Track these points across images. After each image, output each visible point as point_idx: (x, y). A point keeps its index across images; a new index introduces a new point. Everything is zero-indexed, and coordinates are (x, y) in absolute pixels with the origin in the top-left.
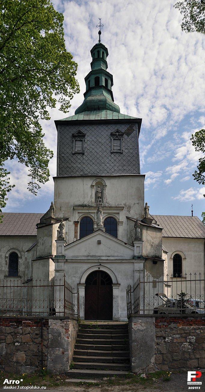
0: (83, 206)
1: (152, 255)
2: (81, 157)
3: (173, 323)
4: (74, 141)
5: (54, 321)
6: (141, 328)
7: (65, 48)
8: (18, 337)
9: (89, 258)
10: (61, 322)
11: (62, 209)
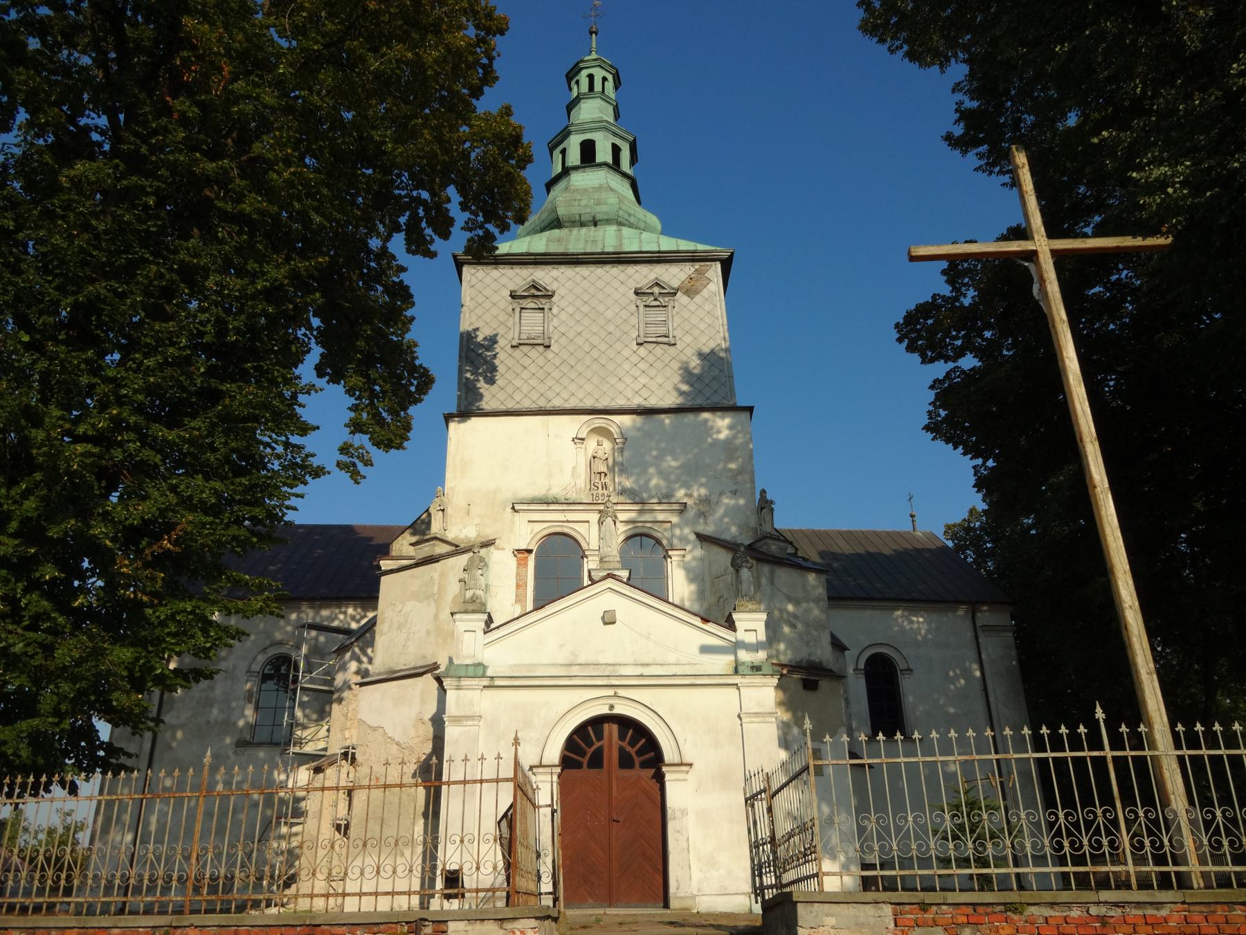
0: (547, 502)
2: (538, 354)
4: (518, 310)
5: (470, 928)
7: (486, 89)
9: (575, 671)
11: (473, 509)
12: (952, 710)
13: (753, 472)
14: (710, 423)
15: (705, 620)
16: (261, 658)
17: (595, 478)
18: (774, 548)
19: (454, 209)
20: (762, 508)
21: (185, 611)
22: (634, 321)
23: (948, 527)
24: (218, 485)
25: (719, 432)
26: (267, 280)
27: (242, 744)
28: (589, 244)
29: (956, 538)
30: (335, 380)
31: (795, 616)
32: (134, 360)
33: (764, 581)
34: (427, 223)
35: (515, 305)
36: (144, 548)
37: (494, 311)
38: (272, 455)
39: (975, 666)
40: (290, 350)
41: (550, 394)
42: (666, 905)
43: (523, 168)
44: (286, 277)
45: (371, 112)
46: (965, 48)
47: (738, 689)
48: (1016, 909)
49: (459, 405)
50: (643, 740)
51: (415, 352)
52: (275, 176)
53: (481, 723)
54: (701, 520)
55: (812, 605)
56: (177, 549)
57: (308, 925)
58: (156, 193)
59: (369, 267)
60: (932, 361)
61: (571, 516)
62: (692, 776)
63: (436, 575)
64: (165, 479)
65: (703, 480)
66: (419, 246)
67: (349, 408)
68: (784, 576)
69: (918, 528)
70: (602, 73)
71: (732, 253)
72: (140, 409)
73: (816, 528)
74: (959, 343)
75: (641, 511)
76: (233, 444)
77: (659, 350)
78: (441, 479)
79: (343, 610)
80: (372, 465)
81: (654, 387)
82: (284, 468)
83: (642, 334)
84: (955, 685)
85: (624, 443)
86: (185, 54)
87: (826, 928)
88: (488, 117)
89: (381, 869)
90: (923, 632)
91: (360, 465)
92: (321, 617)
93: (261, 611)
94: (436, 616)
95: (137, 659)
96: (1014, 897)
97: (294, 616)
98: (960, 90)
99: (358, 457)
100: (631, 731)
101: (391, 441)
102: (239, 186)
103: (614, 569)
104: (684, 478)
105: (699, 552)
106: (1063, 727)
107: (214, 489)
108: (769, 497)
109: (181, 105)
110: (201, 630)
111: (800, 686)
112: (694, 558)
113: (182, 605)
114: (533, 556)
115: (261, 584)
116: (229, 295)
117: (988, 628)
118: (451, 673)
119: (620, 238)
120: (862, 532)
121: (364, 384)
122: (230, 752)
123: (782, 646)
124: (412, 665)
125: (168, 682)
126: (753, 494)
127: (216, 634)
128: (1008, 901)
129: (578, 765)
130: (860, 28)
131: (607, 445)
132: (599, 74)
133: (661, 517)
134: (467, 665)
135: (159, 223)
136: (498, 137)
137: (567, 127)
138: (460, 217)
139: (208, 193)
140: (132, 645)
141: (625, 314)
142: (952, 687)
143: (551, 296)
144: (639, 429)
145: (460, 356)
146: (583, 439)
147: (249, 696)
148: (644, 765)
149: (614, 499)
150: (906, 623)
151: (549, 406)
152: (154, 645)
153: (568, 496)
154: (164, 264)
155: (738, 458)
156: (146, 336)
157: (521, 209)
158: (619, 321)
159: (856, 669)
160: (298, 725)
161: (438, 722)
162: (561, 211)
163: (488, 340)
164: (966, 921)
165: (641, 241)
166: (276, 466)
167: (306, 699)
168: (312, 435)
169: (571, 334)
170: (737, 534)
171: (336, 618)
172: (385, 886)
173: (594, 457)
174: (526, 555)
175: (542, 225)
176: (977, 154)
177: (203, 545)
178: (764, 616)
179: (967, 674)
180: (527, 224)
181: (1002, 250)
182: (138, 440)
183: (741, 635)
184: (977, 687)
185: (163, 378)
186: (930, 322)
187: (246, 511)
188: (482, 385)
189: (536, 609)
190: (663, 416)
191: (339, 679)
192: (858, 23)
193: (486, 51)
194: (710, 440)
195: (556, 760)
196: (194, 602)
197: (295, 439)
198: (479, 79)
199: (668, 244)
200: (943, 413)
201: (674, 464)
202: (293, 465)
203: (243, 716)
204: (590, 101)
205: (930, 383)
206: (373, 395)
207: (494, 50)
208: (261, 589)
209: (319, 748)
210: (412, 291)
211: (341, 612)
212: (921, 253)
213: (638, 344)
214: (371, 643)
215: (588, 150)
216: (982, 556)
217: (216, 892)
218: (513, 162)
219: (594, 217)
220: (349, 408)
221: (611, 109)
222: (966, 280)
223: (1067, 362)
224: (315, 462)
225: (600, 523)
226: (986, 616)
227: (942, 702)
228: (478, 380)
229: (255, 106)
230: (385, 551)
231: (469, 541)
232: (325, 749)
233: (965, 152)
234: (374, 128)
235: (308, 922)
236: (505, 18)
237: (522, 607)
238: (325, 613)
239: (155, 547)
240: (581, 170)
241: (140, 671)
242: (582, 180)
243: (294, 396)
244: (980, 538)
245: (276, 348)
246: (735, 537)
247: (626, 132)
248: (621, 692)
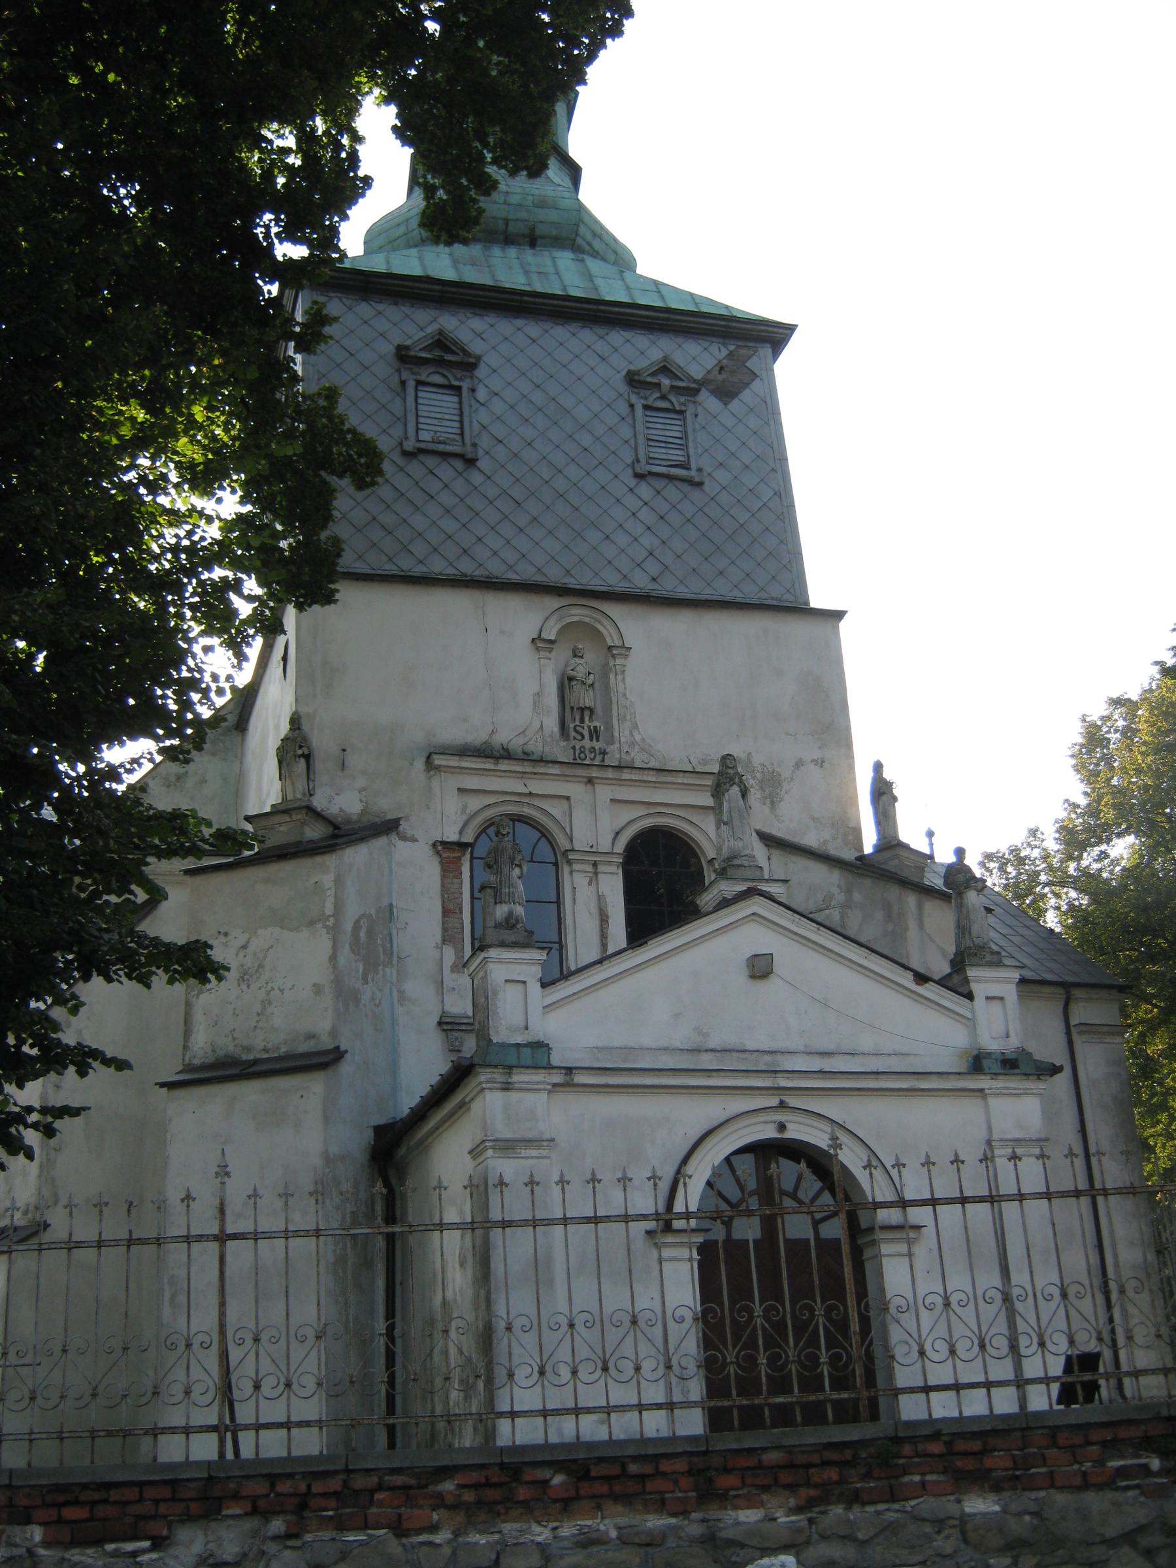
4: (411, 385)
11: (352, 760)
22: (625, 431)
35: (405, 375)
61: (537, 787)
63: (328, 880)
77: (672, 492)
94: (333, 958)
134: (518, 1045)
146: (552, 642)
153: (530, 748)
173: (571, 679)
237: (456, 952)
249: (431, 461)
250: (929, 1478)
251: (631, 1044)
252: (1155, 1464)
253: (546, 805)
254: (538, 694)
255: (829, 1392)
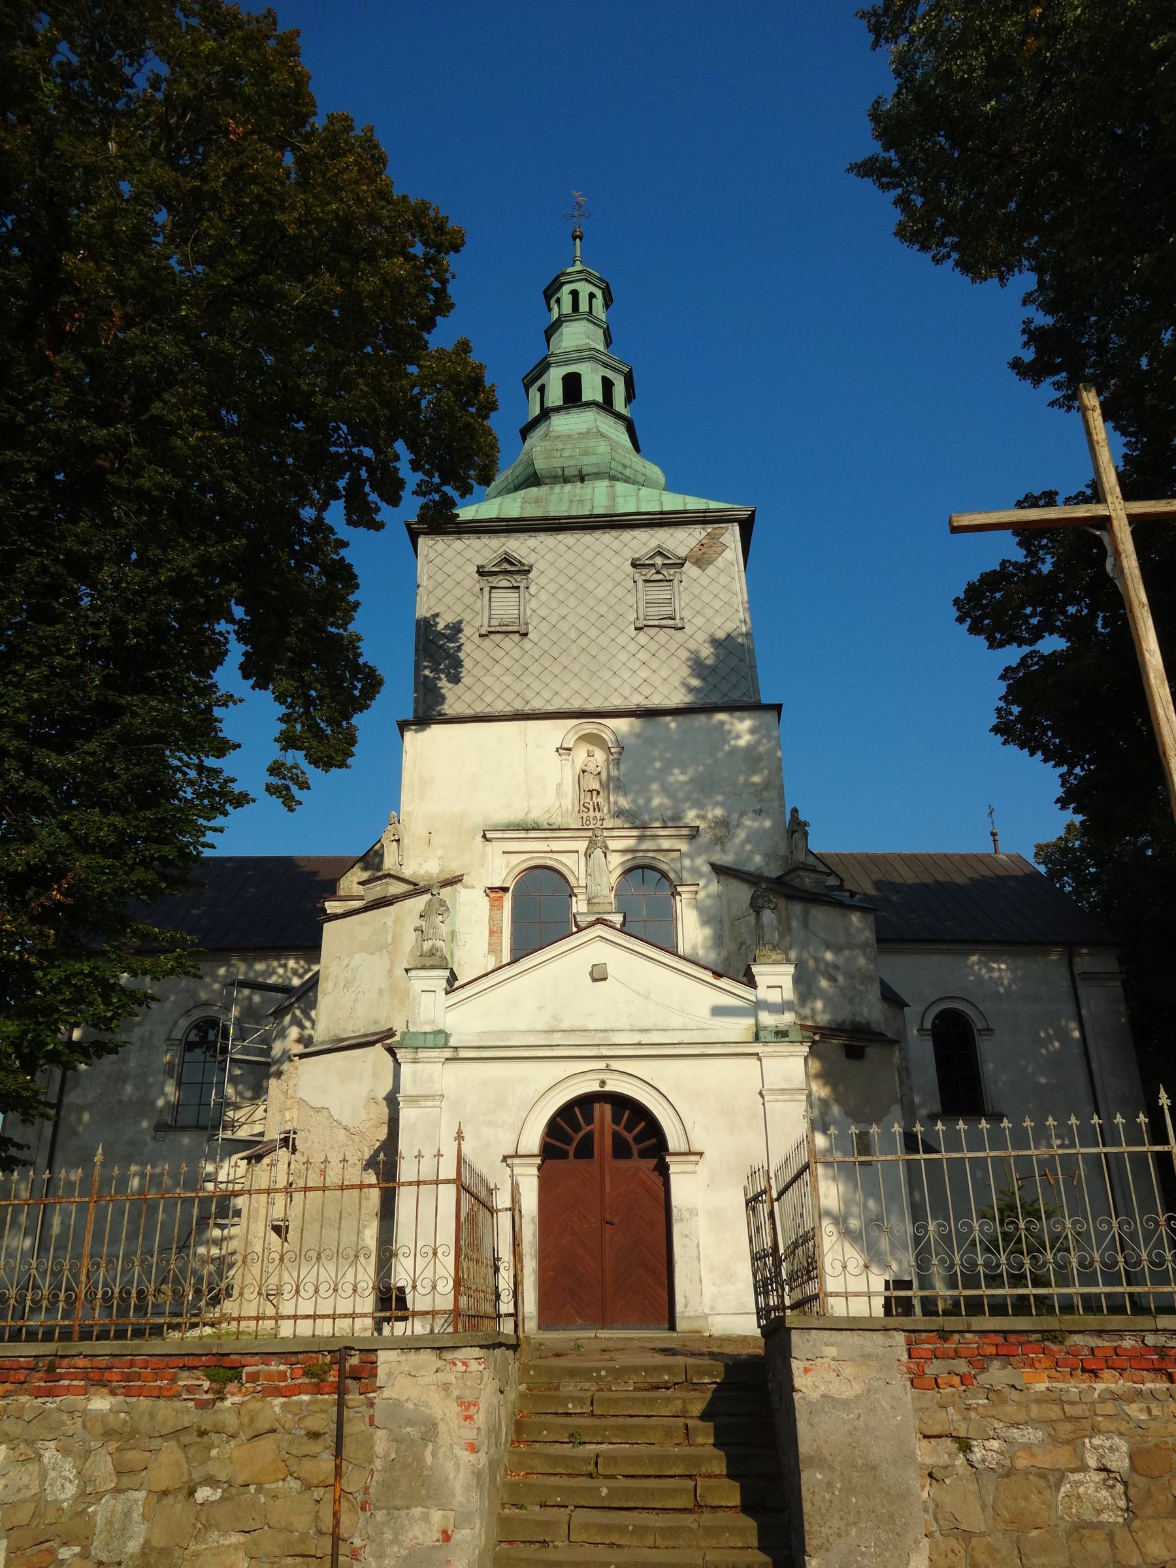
0: (526, 828)
1: (840, 1020)
2: (513, 644)
3: (996, 1364)
4: (487, 589)
5: (403, 1358)
6: (844, 1391)
7: (439, 319)
8: (214, 1452)
9: (557, 1039)
10: (440, 1363)
11: (435, 839)
12: (1043, 1080)
13: (782, 787)
14: (727, 727)
15: (718, 975)
16: (184, 1023)
17: (586, 797)
18: (808, 881)
19: (404, 468)
20: (793, 832)
21: (82, 972)
22: (630, 599)
23: (1040, 848)
24: (117, 820)
25: (738, 737)
26: (172, 570)
27: (162, 1128)
28: (575, 504)
29: (1050, 861)
30: (261, 685)
31: (835, 967)
32: (15, 673)
33: (795, 924)
34: (371, 486)
35: (483, 584)
36: (30, 900)
37: (458, 592)
38: (183, 781)
39: (1073, 1025)
40: (203, 652)
41: (529, 694)
42: (672, 1327)
43: (486, 417)
44: (194, 566)
45: (295, 357)
46: (1032, 254)
47: (760, 1059)
48: (1056, 1338)
49: (416, 710)
50: (643, 1124)
51: (359, 648)
52: (179, 442)
53: (443, 1104)
54: (718, 848)
55: (857, 952)
56: (70, 901)
57: (214, 1355)
58: (37, 468)
59: (301, 543)
60: (1001, 645)
62: (703, 1167)
63: (390, 921)
64: (55, 815)
65: (720, 798)
66: (362, 516)
67: (279, 719)
68: (820, 915)
69: (1001, 849)
70: (591, 289)
71: (753, 512)
72: (20, 731)
73: (871, 851)
74: (1034, 621)
75: (641, 838)
76: (136, 770)
77: (662, 636)
78: (394, 801)
79: (283, 962)
80: (308, 788)
81: (656, 680)
82: (200, 796)
83: (641, 617)
84: (1047, 1049)
85: (620, 753)
86: (66, 299)
87: (825, 1360)
88: (441, 354)
89: (301, 1288)
90: (1006, 982)
91: (294, 789)
92: (255, 971)
93: (171, 972)
94: (390, 971)
95: (25, 1032)
96: (1050, 1323)
97: (222, 971)
98: (1033, 302)
99: (292, 779)
100: (627, 1112)
101: (331, 758)
102: (136, 455)
103: (605, 913)
104: (695, 796)
105: (715, 887)
106: (1118, 1116)
107: (114, 825)
108: (802, 817)
109: (64, 360)
110: (101, 995)
111: (841, 1054)
112: (709, 896)
113: (78, 966)
114: (509, 895)
115: (173, 938)
116: (127, 588)
117: (1088, 976)
118: (407, 1043)
119: (613, 497)
120: (929, 855)
121: (296, 689)
122: (149, 1138)
123: (819, 1005)
124: (361, 1032)
125: (64, 1059)
126: (783, 813)
127: (120, 1000)
128: (1045, 1328)
129: (563, 1155)
130: (896, 234)
131: (600, 756)
132: (584, 289)
133: (666, 844)
135: (41, 505)
136: (453, 381)
137: (546, 358)
138: (411, 478)
139: (101, 462)
140: (19, 1016)
141: (619, 591)
142: (1043, 1051)
143: (528, 571)
144: (638, 736)
145: (416, 650)
146: (569, 749)
147: (169, 1070)
148: (643, 1154)
149: (609, 823)
150: (984, 971)
151: (527, 709)
152: (46, 1016)
153: (552, 821)
154: (48, 554)
155: (763, 768)
156: (28, 642)
157: (485, 466)
158: (613, 601)
159: (921, 1030)
160: (228, 1105)
161: (392, 1101)
162: (540, 465)
163: (451, 628)
164: (994, 1352)
165: (638, 500)
166: (189, 794)
167: (238, 1072)
168: (232, 755)
169: (554, 619)
170: (763, 864)
171: (274, 972)
172: (306, 1308)
173: (584, 772)
174: (501, 894)
175: (516, 482)
176: (1054, 384)
177: (102, 894)
178: (791, 969)
179: (1062, 1035)
180: (493, 484)
181: (1067, 516)
182: (22, 768)
183: (763, 993)
184: (1076, 1051)
185: (49, 694)
186: (998, 595)
187: (154, 850)
188: (443, 683)
189: (514, 961)
190: (668, 718)
191: (277, 1048)
192: (894, 228)
193: (437, 273)
194: (727, 747)
195: (536, 1150)
196: (92, 964)
197: (210, 762)
198: (431, 308)
199: (673, 502)
200: (1016, 709)
201: (682, 778)
202: (210, 793)
203: (163, 1094)
204: (575, 324)
205: (1001, 672)
206: (308, 702)
207: (447, 271)
208: (173, 944)
209: (255, 1132)
210: (356, 570)
211: (280, 966)
212: (965, 523)
213: (636, 629)
214: (313, 1005)
215: (572, 385)
216: (1083, 883)
217: (110, 1315)
218: (473, 410)
219: (580, 471)
220: (279, 719)
221: (600, 332)
222: (1044, 542)
223: (1147, 655)
224: (237, 788)
225: (588, 855)
226: (1086, 961)
227: (1030, 1070)
228: (440, 679)
229: (153, 356)
230: (330, 889)
231: (431, 878)
232: (262, 1134)
233: (1037, 382)
234: (299, 375)
235: (214, 1351)
236: (460, 231)
238: (260, 967)
239: (43, 899)
240: (563, 412)
241: (29, 1046)
242: (565, 424)
243: (209, 709)
244: (1082, 860)
245: (185, 651)
246: (760, 868)
247: (620, 362)
248: (615, 1065)
249: (497, 638)
250: (74, 1383)
251: (508, 1028)
252: (206, 1385)
253: (562, 857)
254: (559, 785)
255: (132, 1317)
